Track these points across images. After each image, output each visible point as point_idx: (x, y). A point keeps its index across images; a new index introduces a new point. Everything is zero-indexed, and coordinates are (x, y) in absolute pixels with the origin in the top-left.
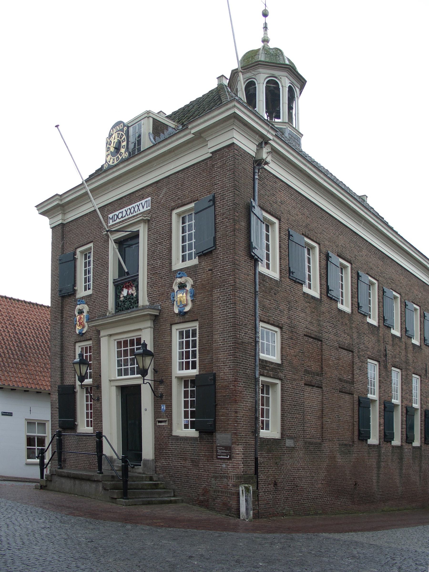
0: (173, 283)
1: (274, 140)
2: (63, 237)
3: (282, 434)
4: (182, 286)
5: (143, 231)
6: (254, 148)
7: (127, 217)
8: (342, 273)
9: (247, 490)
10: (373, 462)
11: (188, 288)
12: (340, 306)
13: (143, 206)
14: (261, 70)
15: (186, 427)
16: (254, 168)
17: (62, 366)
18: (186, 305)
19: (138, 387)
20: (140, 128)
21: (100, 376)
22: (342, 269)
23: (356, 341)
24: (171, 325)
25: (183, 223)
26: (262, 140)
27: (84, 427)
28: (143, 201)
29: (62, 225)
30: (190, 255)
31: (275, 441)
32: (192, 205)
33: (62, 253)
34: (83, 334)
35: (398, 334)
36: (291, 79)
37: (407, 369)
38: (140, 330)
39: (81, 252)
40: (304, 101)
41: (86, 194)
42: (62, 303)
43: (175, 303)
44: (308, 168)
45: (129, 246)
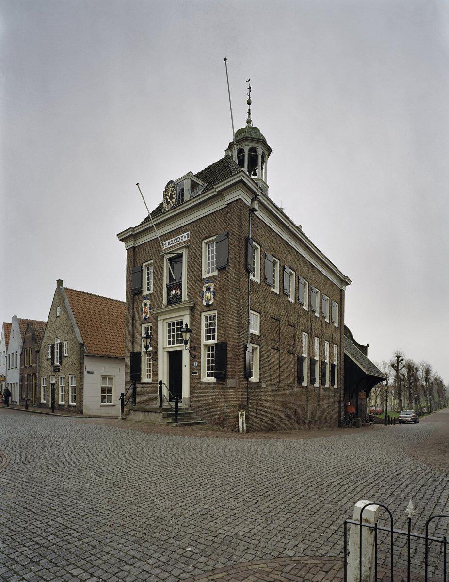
0: (203, 286)
1: (260, 196)
2: (133, 253)
3: (260, 379)
4: (208, 289)
5: (185, 252)
6: (250, 201)
7: (175, 244)
8: (274, 267)
9: (243, 415)
10: (304, 396)
11: (212, 290)
12: (272, 289)
13: (185, 237)
14: (246, 143)
15: (208, 376)
16: (250, 214)
17: (133, 340)
18: (210, 300)
19: (181, 351)
20: (183, 185)
21: (158, 345)
22: (274, 264)
23: (297, 321)
24: (201, 312)
25: (208, 249)
26: (254, 196)
27: (145, 379)
28: (185, 234)
29: (134, 248)
30: (212, 269)
31: (257, 383)
32: (215, 237)
33: (134, 266)
34: (147, 319)
35: (318, 315)
36: (264, 149)
37: (323, 338)
38: (183, 316)
39: (146, 266)
40: (270, 160)
41: (152, 226)
42: (134, 298)
43: (204, 299)
44: (277, 213)
45: (176, 263)
